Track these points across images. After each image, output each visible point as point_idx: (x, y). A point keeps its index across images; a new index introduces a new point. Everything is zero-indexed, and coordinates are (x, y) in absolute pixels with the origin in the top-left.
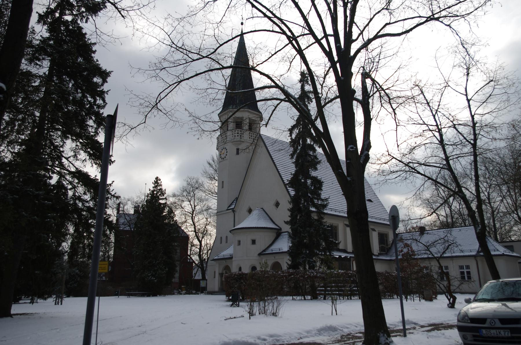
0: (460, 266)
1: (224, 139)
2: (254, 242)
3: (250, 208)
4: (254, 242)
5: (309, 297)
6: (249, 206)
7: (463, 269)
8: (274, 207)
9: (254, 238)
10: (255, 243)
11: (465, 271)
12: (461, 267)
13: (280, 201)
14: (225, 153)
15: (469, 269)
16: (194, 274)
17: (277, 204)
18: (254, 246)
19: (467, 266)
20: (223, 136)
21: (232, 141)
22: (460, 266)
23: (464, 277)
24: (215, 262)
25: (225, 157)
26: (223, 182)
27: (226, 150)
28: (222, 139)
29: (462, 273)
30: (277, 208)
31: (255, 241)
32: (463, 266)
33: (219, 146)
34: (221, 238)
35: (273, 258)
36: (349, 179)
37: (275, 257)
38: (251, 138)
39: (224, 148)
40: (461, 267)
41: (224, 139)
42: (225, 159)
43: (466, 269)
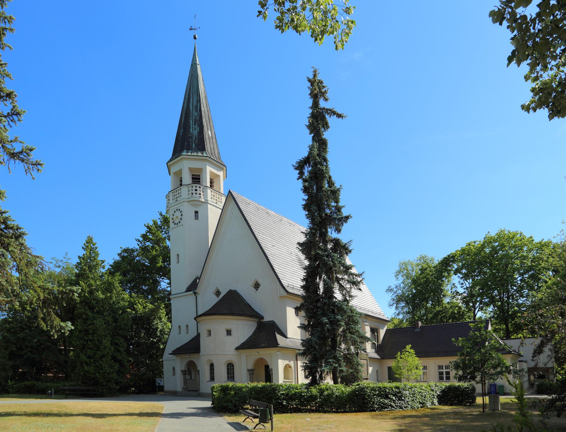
0: (439, 366)
1: (177, 197)
2: (229, 333)
3: (218, 290)
4: (229, 333)
5: (244, 390)
6: (217, 288)
7: (443, 369)
8: (254, 289)
9: (229, 327)
10: (231, 334)
11: (444, 371)
12: (440, 367)
13: (260, 282)
14: (180, 217)
15: (426, 369)
16: (299, 351)
17: (257, 286)
18: (229, 337)
19: (441, 366)
20: (176, 194)
21: (189, 200)
22: (439, 366)
23: (443, 377)
24: (175, 356)
25: (180, 222)
26: (178, 255)
27: (181, 212)
28: (174, 198)
29: (441, 373)
30: (257, 290)
31: (230, 331)
32: (443, 366)
33: (170, 206)
34: (180, 327)
35: (257, 353)
36: (142, 387)
37: (258, 353)
38: (214, 199)
39: (177, 210)
40: (440, 367)
41: (177, 197)
42: (179, 224)
43: (446, 369)
